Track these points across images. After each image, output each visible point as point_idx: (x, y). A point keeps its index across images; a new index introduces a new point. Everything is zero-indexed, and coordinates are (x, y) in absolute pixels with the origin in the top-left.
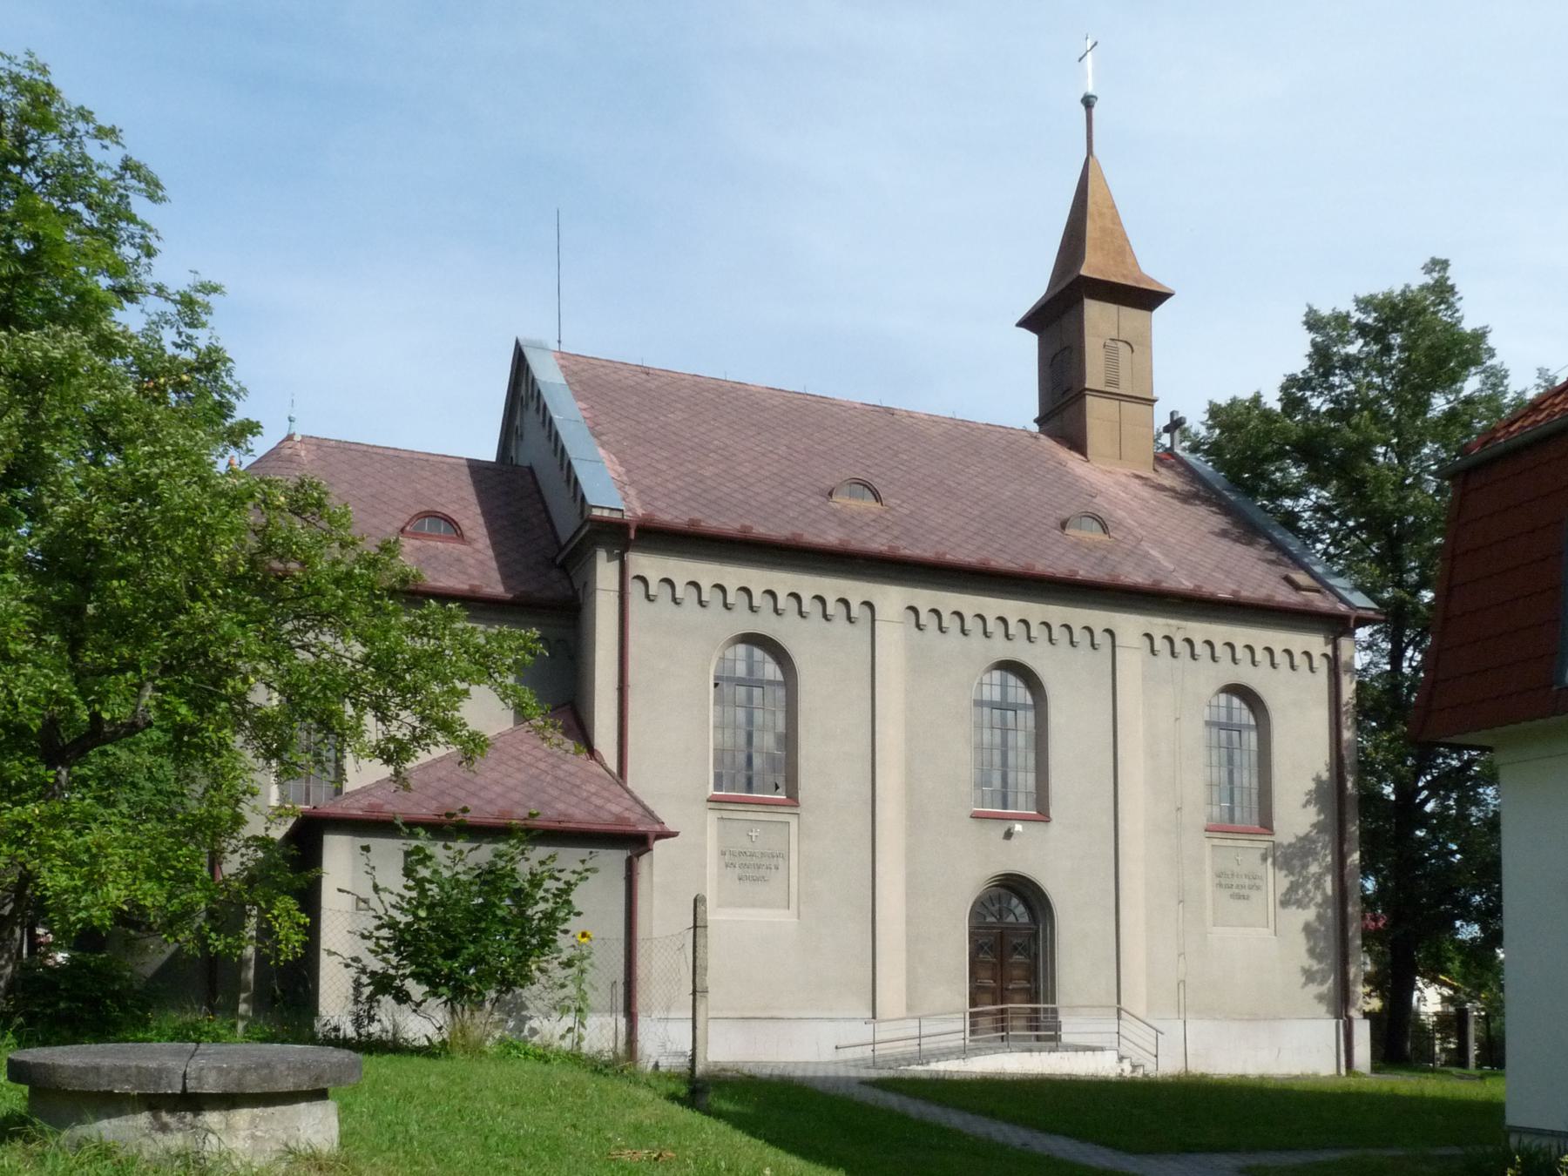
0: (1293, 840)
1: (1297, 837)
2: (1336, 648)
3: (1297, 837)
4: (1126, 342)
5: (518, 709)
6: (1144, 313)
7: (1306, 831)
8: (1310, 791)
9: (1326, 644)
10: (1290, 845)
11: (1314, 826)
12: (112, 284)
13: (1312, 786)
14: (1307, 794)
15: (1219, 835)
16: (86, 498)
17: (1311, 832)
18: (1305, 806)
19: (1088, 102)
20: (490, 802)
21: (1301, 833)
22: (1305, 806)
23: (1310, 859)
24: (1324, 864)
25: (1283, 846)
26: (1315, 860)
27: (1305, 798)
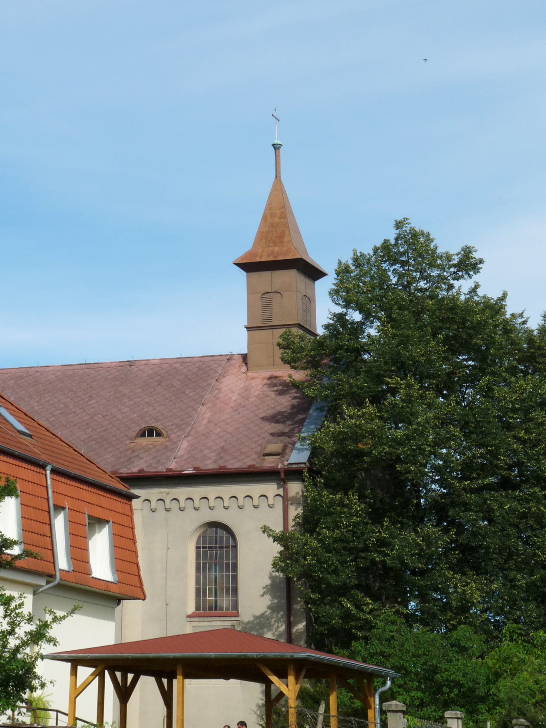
0: (251, 619)
1: (254, 616)
2: (286, 491)
3: (254, 616)
4: (309, 298)
5: (426, 440)
6: (308, 281)
7: (262, 612)
8: (267, 586)
9: (278, 488)
10: (248, 622)
11: (269, 607)
12: (525, 325)
13: (269, 582)
14: (264, 588)
15: (197, 619)
16: (380, 289)
17: (266, 612)
18: (262, 596)
19: (276, 147)
20: (206, 465)
21: (258, 614)
22: (262, 596)
23: (265, 630)
24: (277, 633)
25: (243, 623)
26: (269, 630)
27: (262, 591)
